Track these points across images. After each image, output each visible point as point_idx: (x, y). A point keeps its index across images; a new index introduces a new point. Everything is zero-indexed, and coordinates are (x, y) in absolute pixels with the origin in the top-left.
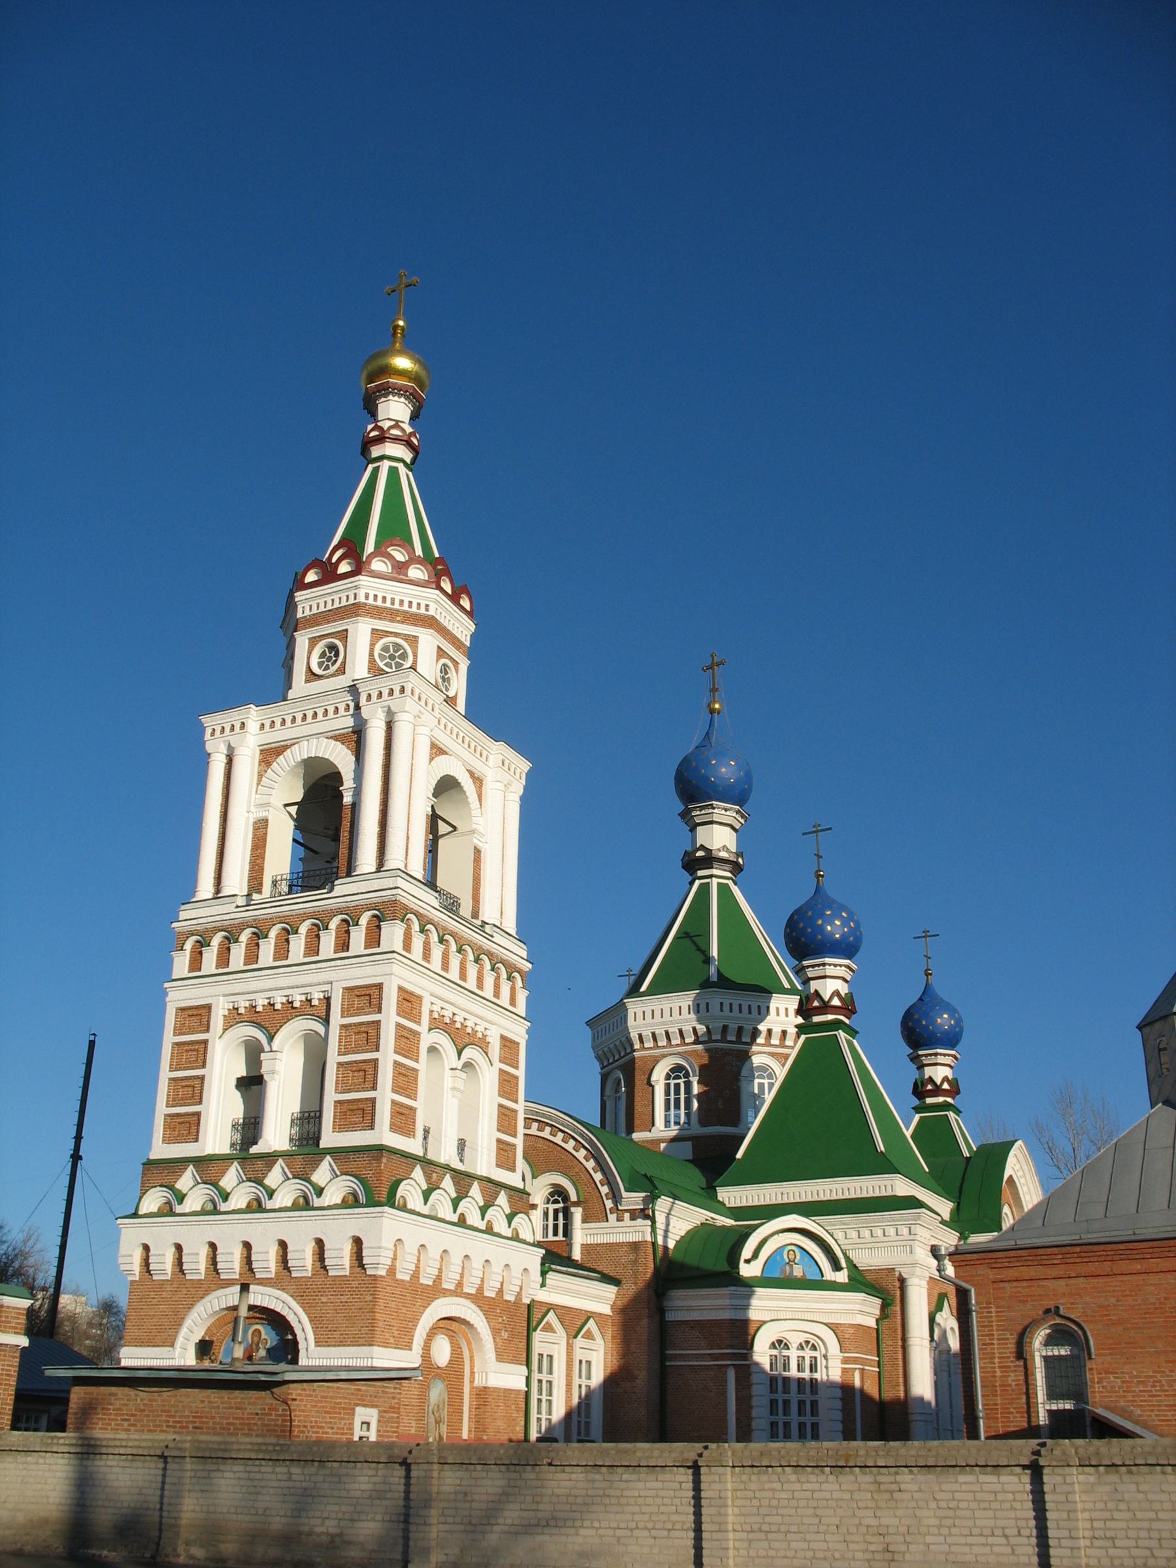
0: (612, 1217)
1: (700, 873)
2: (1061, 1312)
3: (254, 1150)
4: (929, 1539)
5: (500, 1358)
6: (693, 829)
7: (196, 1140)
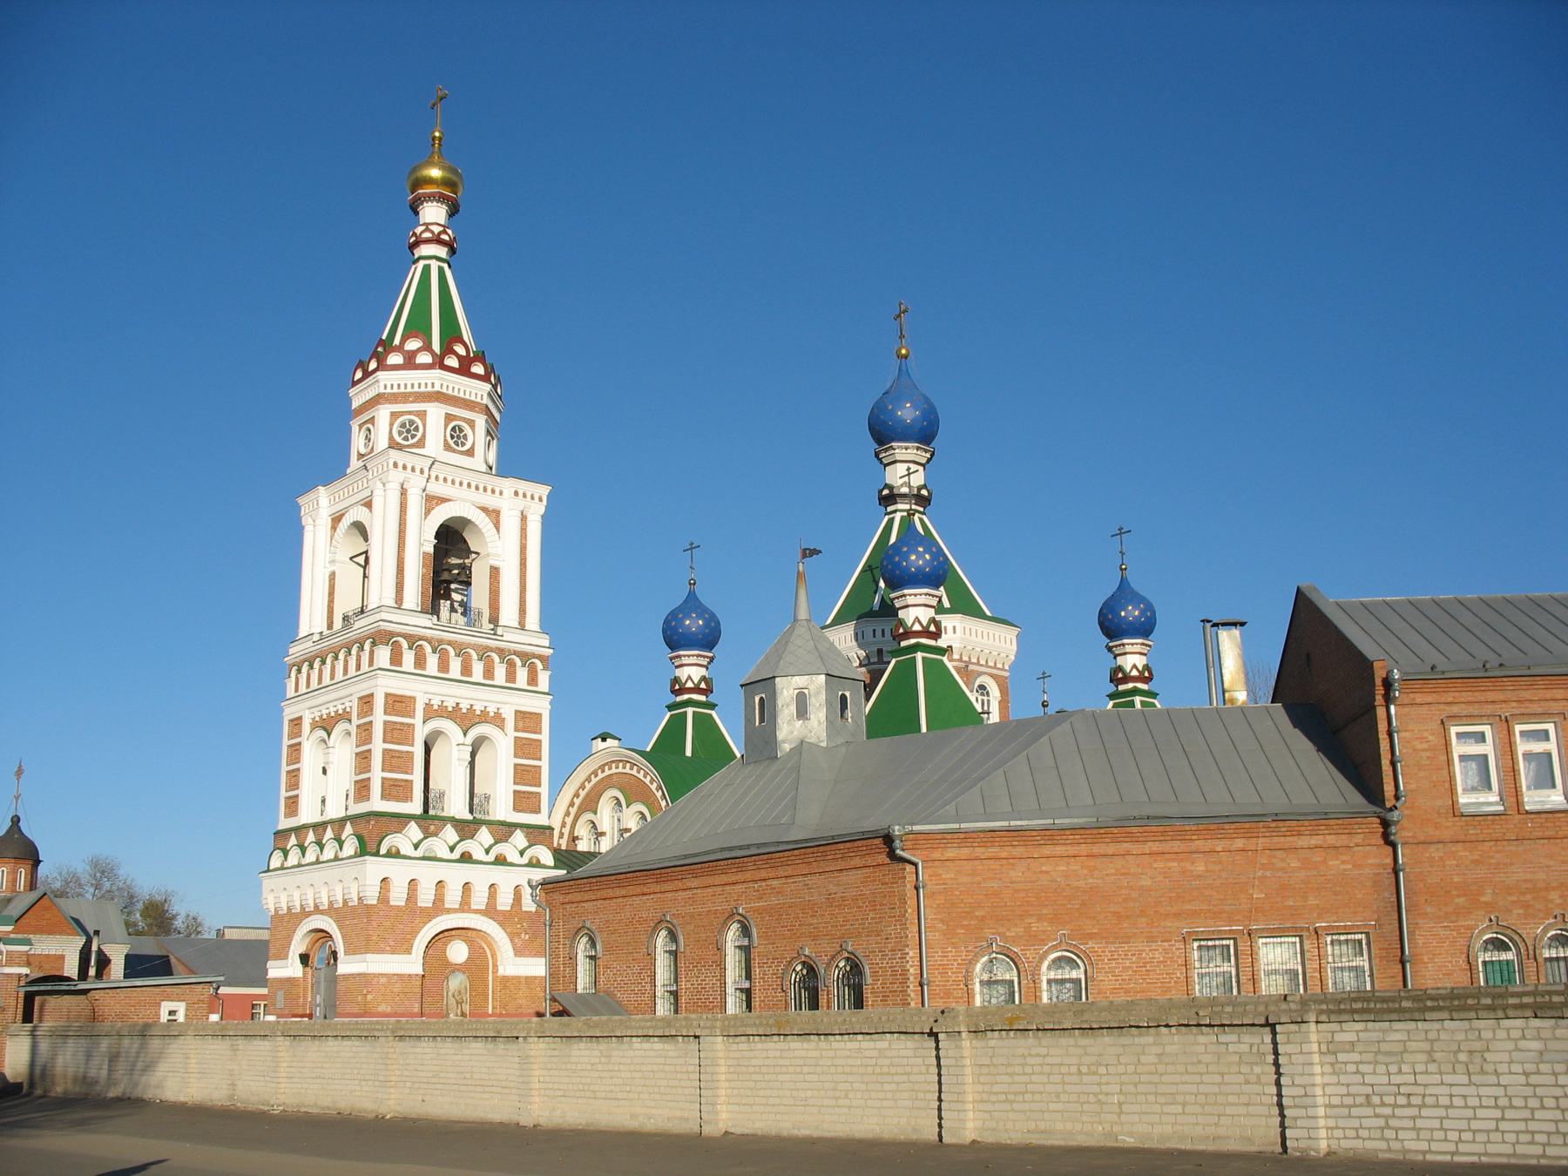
5: (519, 952)
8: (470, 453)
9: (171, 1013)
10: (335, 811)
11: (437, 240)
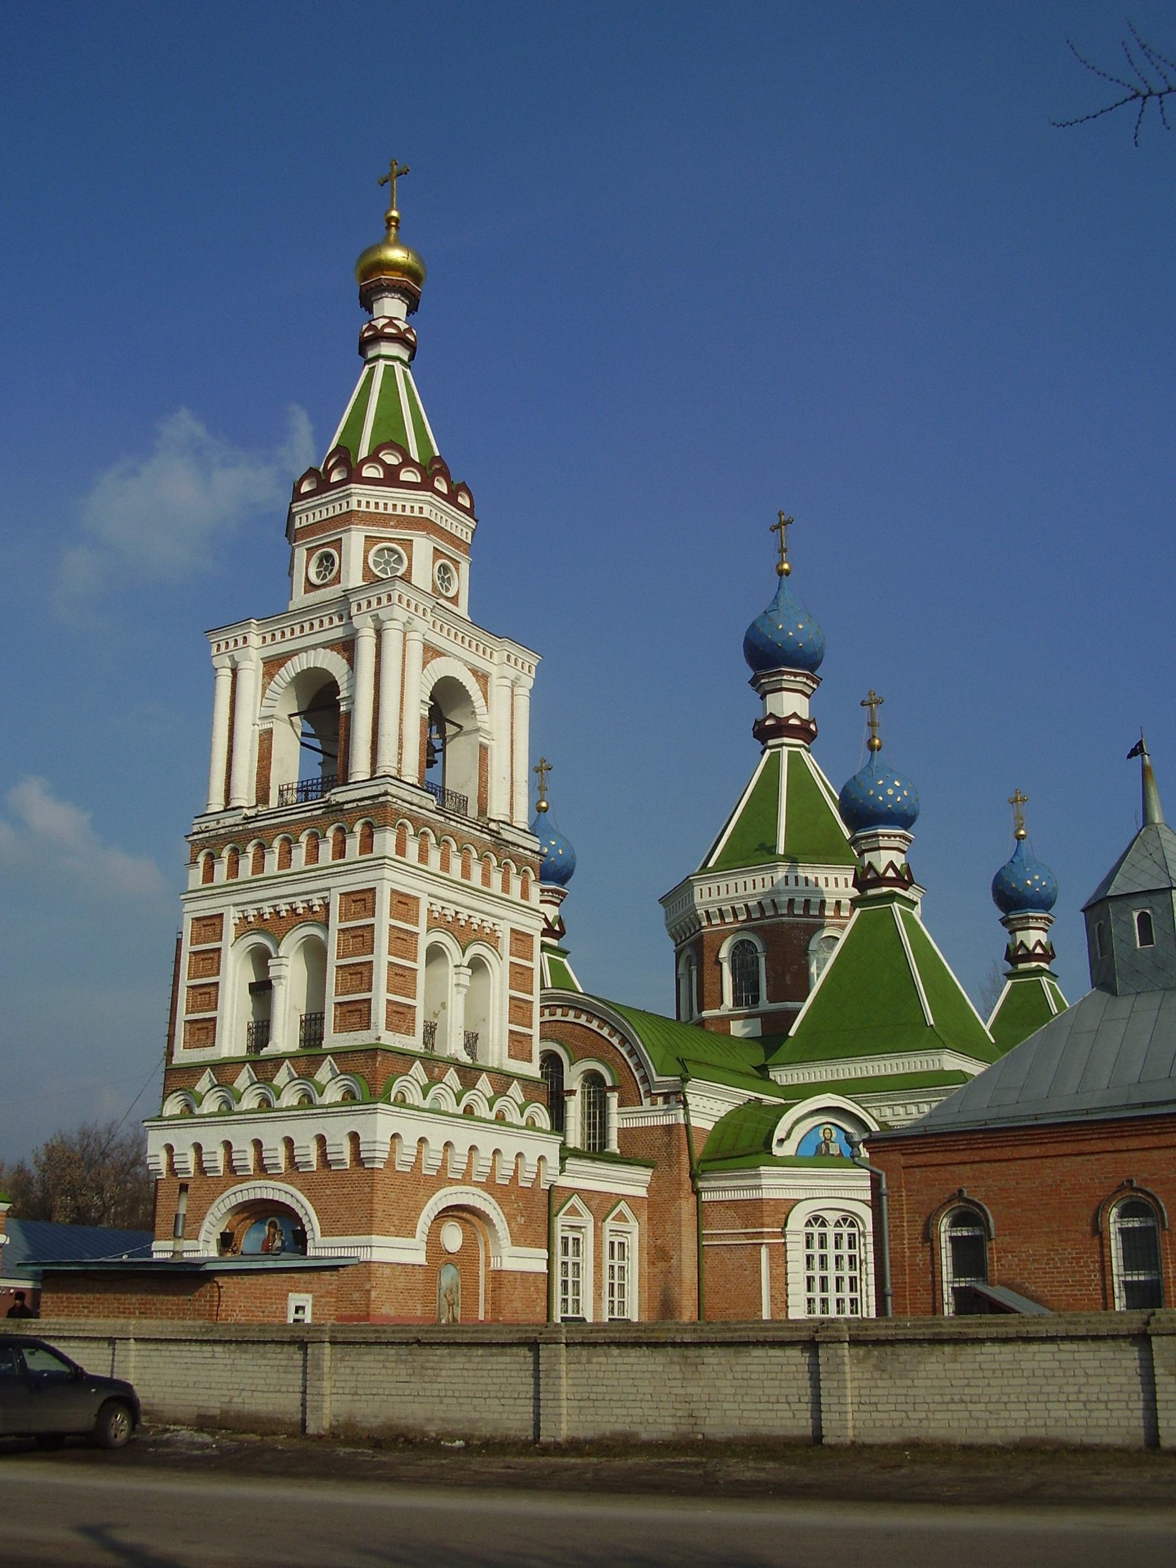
0: (647, 1102)
1: (771, 742)
2: (965, 1195)
3: (265, 1052)
4: (726, 1406)
5: (515, 1242)
6: (763, 697)
7: (213, 1044)
9: (298, 1309)
11: (399, 339)
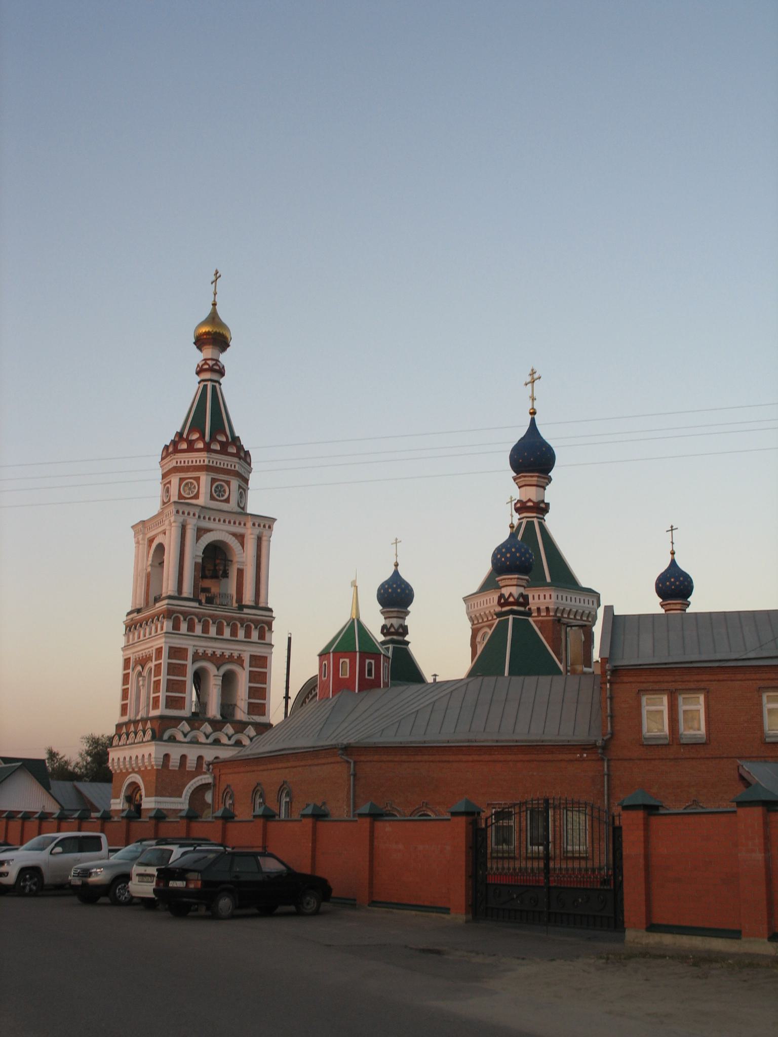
8: (227, 501)
10: (142, 714)
